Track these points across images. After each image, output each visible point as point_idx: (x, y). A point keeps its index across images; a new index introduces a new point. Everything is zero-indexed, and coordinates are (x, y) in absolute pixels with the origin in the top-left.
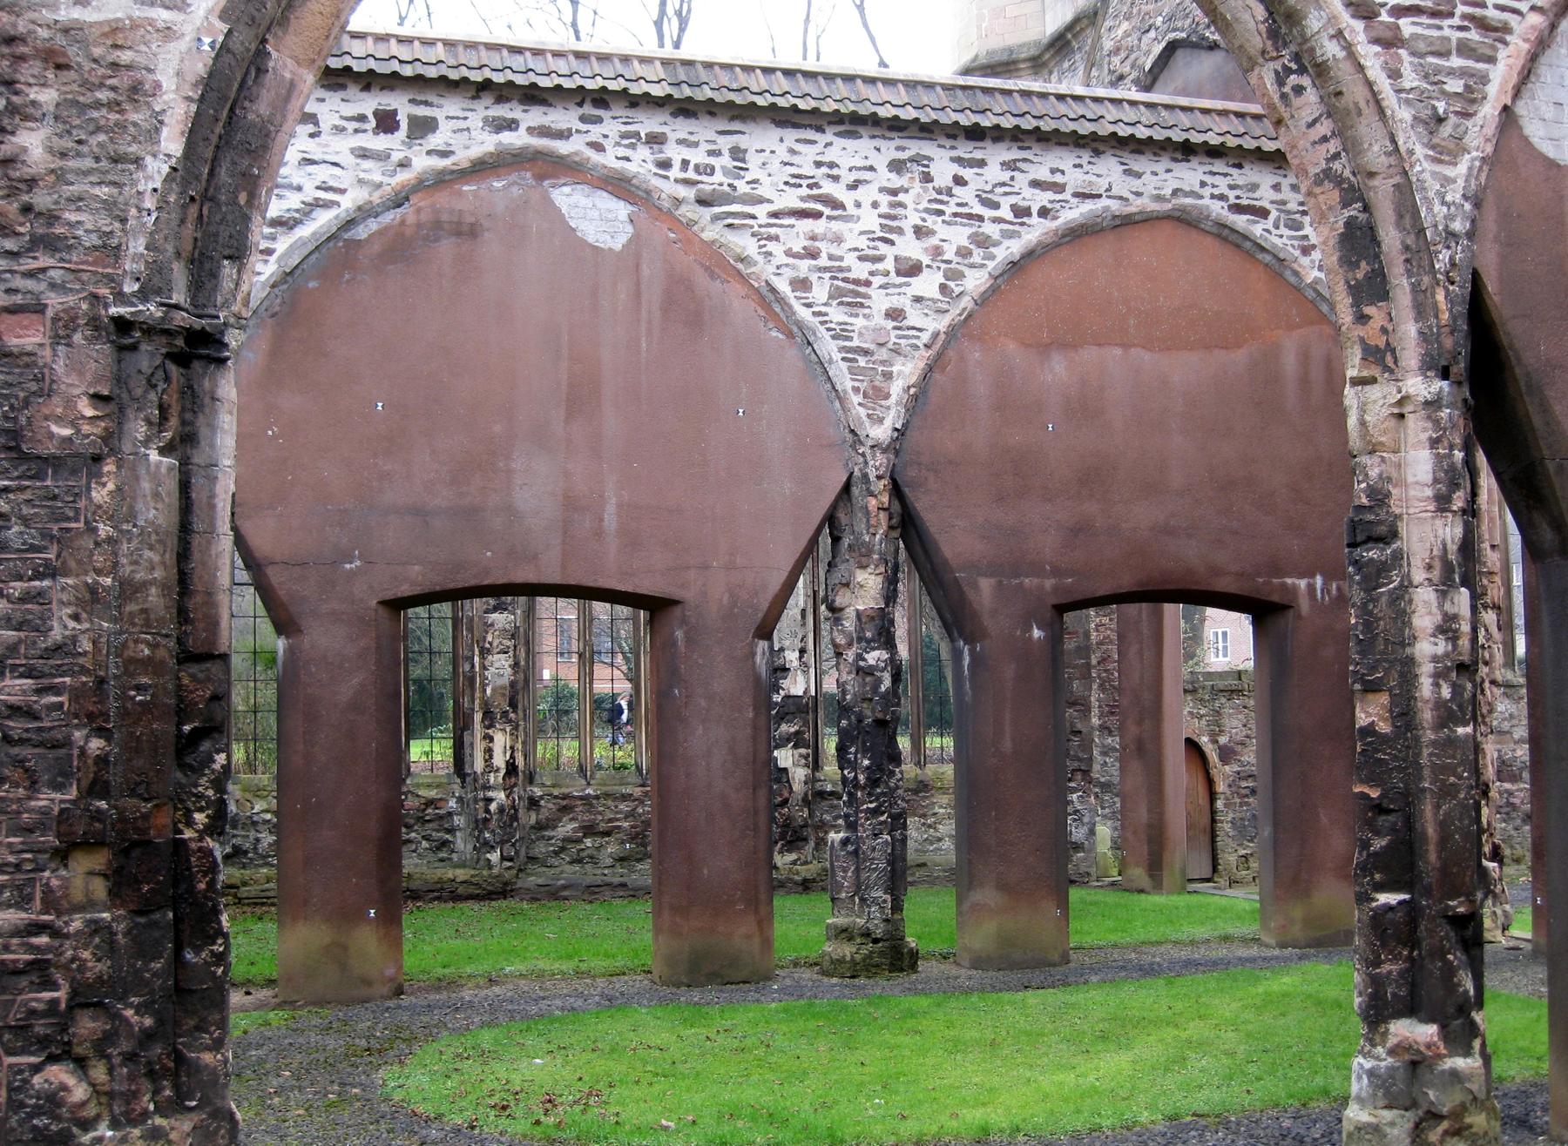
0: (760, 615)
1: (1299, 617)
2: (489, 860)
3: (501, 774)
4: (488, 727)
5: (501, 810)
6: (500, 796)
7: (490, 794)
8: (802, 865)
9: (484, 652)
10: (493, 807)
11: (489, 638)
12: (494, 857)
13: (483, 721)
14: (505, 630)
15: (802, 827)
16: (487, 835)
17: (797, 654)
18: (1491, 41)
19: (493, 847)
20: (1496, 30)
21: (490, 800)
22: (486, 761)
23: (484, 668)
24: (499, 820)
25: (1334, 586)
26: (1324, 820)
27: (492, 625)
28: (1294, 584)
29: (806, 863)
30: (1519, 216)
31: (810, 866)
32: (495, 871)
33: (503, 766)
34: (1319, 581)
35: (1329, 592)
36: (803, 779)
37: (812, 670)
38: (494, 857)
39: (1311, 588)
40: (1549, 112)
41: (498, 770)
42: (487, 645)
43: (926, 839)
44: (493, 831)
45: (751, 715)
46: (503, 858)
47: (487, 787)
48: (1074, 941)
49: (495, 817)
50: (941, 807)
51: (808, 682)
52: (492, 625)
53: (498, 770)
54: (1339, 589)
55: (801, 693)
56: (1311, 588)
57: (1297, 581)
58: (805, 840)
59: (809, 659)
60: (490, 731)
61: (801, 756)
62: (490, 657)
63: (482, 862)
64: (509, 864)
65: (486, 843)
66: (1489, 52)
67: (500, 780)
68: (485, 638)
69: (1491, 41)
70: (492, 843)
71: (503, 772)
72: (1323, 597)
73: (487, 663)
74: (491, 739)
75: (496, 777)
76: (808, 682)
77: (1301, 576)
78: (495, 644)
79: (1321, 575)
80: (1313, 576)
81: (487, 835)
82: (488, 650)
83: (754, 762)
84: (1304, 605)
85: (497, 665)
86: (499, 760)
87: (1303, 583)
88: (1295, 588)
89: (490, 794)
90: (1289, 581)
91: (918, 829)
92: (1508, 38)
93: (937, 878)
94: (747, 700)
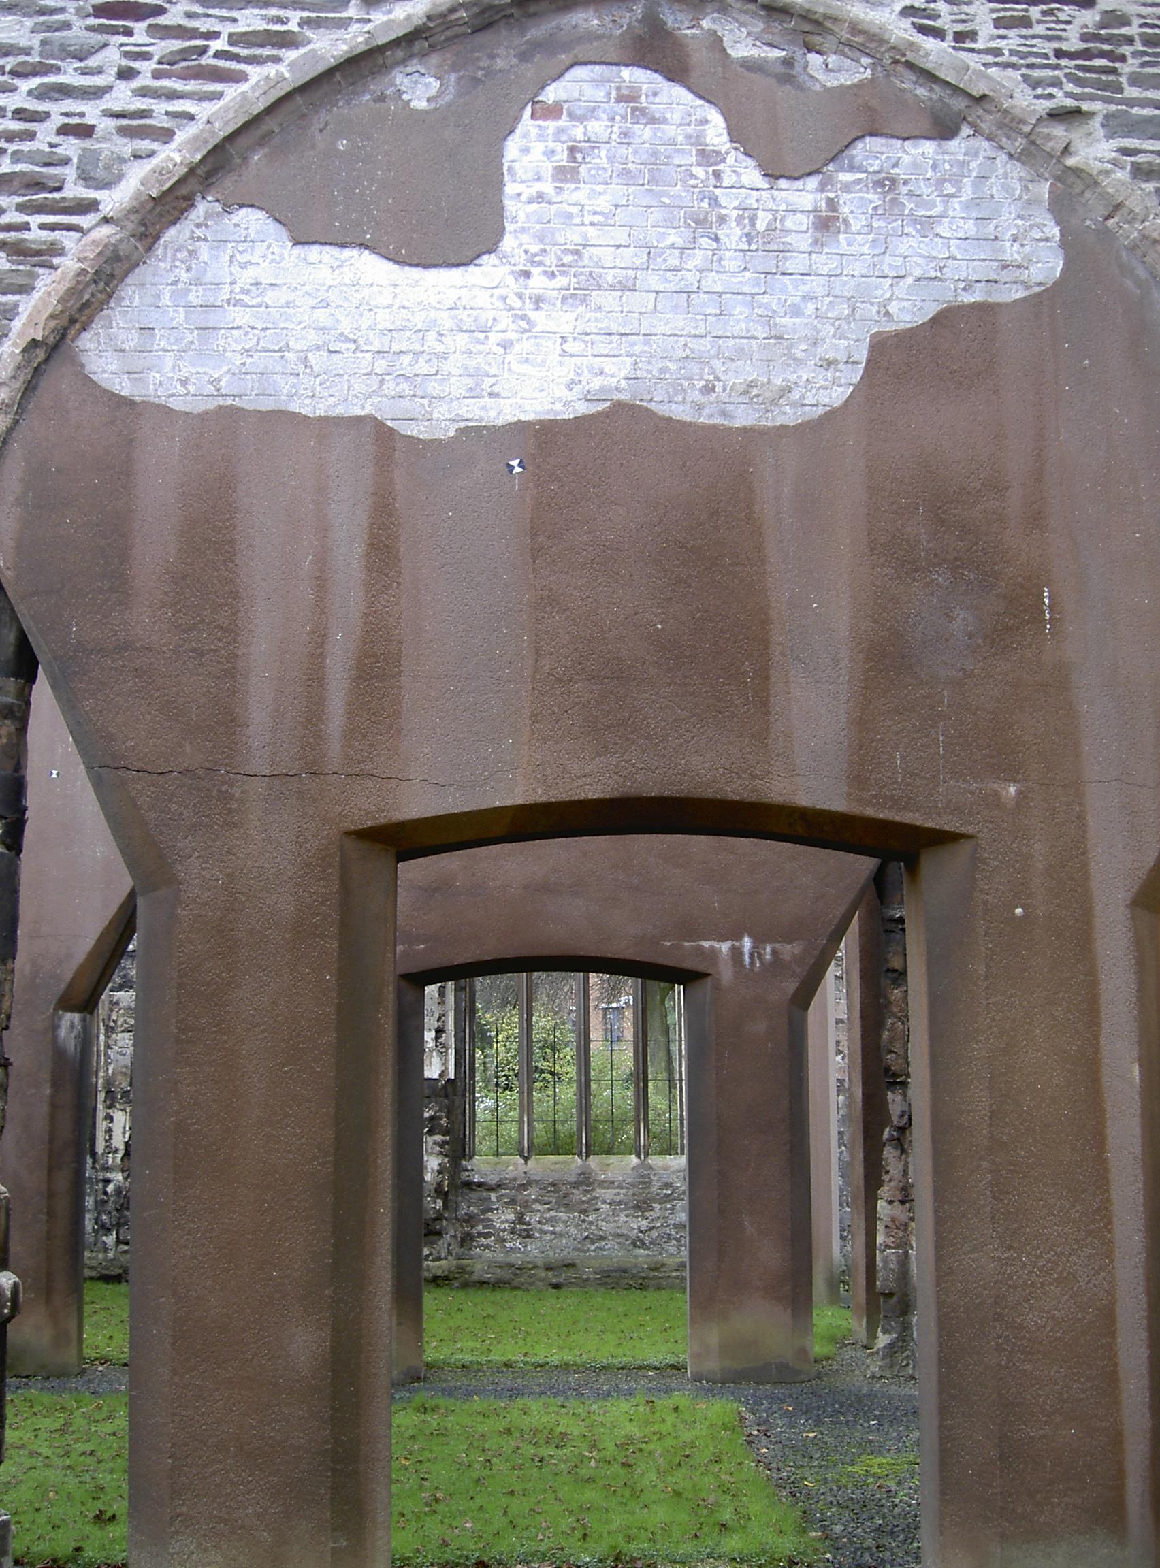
0: (63, 986)
1: (717, 987)
2: (105, 1244)
3: (119, 1156)
4: (109, 1107)
5: (118, 1191)
6: (118, 1177)
7: (108, 1175)
8: (433, 1260)
9: (110, 1030)
10: (110, 1188)
11: (114, 1017)
12: (110, 1240)
13: (105, 1101)
14: (130, 1008)
15: (435, 1219)
16: (104, 1217)
17: (433, 1034)
18: (28, 268)
19: (109, 1230)
20: (39, 253)
21: (107, 1181)
22: (106, 1141)
23: (108, 1047)
24: (115, 1202)
25: (768, 948)
26: (750, 1228)
27: (117, 1003)
28: (712, 947)
29: (439, 1259)
30: (59, 471)
31: (443, 1262)
32: (111, 1255)
33: (122, 1147)
34: (747, 943)
35: (760, 957)
36: (436, 1168)
37: (452, 1052)
38: (110, 1240)
39: (736, 953)
40: (131, 340)
41: (116, 1151)
42: (112, 1024)
43: (587, 1237)
44: (110, 1213)
45: (48, 1091)
46: (119, 1241)
47: (107, 1169)
48: (430, 1355)
49: (112, 1199)
50: (604, 1202)
51: (445, 1064)
52: (117, 1003)
53: (116, 1151)
54: (774, 952)
55: (436, 1076)
56: (736, 953)
57: (716, 945)
58: (439, 1234)
59: (448, 1038)
60: (110, 1111)
61: (435, 1143)
62: (114, 1036)
63: (99, 1245)
64: (126, 1248)
65: (103, 1226)
66: (21, 281)
67: (118, 1161)
68: (110, 1016)
69: (28, 268)
70: (108, 1225)
71: (121, 1153)
72: (752, 963)
73: (111, 1042)
74: (111, 1119)
75: (114, 1158)
76: (445, 1064)
77: (722, 939)
78: (119, 1023)
79: (750, 936)
80: (739, 938)
81: (104, 1217)
82: (113, 1028)
83: (51, 1141)
84: (726, 973)
85: (120, 1044)
86: (119, 1141)
87: (725, 947)
88: (713, 954)
89: (108, 1175)
90: (706, 944)
91: (577, 1226)
92: (56, 261)
93: (587, 1280)
94: (46, 1075)
